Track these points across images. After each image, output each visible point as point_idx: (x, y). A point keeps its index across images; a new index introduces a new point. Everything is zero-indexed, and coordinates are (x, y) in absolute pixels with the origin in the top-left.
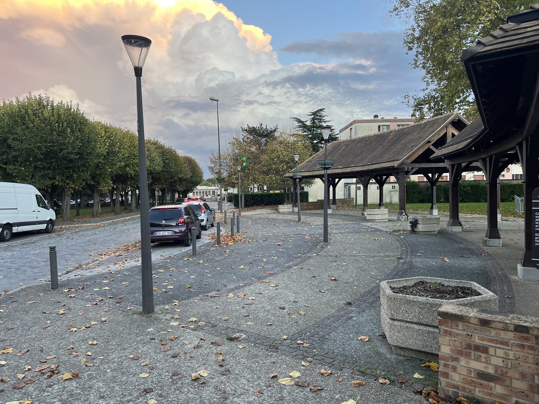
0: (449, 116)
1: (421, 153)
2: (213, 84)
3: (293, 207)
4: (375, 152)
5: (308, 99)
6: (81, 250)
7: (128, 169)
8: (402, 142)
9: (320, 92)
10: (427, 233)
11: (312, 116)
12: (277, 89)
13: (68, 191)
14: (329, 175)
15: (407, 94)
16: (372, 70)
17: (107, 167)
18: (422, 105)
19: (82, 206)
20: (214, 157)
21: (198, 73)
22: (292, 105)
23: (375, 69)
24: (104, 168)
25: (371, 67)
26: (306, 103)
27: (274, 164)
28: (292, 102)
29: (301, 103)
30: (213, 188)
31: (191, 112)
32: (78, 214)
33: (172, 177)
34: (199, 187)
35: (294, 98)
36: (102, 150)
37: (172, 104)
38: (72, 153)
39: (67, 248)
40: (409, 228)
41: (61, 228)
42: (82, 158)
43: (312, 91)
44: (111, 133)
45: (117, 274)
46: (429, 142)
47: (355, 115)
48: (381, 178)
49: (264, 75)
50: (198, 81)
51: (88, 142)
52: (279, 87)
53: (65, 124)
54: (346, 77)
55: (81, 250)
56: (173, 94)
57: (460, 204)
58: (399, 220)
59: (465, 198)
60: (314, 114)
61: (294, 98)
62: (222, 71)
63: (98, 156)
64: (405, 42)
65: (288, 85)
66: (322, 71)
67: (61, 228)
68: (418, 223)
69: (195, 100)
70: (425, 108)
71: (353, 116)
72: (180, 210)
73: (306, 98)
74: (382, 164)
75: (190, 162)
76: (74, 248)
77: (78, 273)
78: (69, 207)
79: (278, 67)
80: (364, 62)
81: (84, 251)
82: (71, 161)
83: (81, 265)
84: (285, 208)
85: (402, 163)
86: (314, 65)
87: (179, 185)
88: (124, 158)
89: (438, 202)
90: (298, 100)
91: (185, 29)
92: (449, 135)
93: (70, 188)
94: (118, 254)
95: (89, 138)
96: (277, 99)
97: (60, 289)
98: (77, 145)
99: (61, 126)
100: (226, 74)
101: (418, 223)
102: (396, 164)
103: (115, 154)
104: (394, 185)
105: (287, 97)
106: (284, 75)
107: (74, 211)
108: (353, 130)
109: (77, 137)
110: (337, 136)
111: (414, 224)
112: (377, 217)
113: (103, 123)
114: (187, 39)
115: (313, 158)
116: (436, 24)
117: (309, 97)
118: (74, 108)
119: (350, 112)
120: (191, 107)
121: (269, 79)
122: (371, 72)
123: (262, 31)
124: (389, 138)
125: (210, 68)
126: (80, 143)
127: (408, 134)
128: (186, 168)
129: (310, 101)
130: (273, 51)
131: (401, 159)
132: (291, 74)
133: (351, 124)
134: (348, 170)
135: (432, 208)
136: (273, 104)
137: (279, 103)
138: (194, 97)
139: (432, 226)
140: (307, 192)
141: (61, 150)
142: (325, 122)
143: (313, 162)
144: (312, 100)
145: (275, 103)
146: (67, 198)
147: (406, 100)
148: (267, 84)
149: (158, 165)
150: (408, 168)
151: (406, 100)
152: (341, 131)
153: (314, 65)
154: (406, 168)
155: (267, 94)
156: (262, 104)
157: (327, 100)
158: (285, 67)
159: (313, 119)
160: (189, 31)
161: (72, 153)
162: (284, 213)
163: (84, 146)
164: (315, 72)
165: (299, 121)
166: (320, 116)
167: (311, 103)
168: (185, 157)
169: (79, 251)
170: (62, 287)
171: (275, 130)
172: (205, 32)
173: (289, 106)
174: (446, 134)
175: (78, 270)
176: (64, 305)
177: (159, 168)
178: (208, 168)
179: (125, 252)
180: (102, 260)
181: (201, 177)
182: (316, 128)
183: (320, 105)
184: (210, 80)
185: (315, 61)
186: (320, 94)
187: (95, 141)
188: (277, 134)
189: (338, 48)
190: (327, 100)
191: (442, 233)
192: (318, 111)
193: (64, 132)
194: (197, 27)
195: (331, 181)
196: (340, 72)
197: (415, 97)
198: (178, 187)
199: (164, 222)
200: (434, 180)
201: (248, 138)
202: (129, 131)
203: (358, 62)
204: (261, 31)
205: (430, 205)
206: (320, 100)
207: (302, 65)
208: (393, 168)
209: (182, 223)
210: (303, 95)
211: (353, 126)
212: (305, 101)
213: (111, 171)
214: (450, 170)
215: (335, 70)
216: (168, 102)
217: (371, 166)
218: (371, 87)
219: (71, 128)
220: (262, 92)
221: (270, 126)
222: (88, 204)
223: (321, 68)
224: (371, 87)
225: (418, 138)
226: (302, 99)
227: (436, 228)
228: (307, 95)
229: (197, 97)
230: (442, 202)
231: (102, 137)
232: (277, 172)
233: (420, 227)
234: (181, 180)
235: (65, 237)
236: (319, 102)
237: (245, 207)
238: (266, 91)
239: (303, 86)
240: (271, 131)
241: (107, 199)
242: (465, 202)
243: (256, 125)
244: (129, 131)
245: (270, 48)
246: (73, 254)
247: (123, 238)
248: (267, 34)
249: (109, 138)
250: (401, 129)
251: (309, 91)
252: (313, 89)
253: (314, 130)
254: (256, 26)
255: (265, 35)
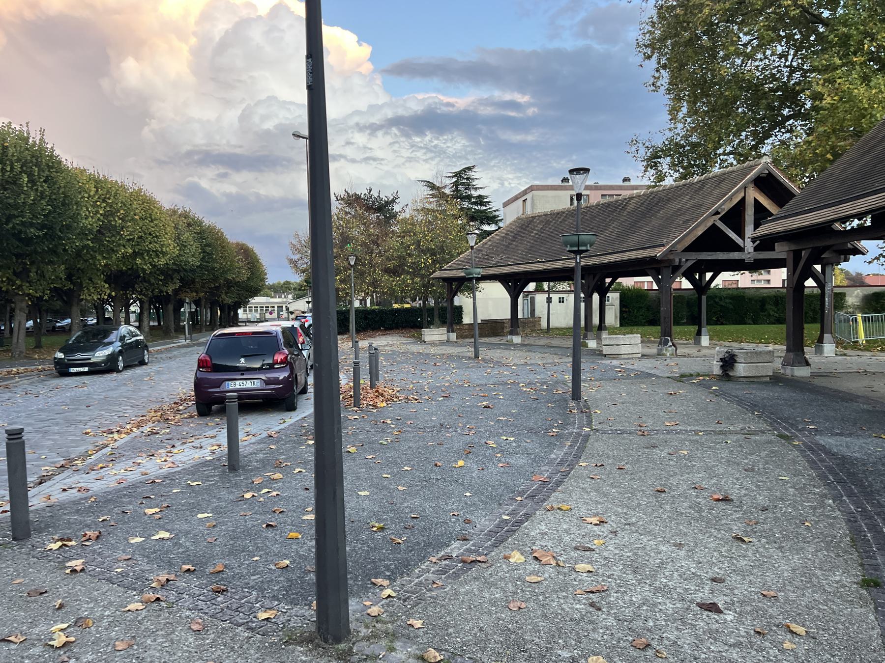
0: (751, 168)
1: (700, 233)
2: (269, 125)
3: (448, 332)
4: (607, 233)
5: (429, 155)
6: (61, 421)
7: (139, 261)
8: (659, 215)
9: (449, 145)
10: (752, 380)
11: (455, 179)
12: (376, 137)
13: (22, 301)
14: (587, 271)
15: (634, 138)
16: (531, 111)
17: (99, 257)
18: (660, 157)
19: (44, 331)
20: (300, 242)
21: (244, 106)
22: (403, 164)
23: (536, 110)
24: (94, 258)
25: (530, 105)
26: (426, 161)
27: (410, 255)
28: (404, 160)
29: (418, 161)
30: (277, 300)
31: (229, 171)
32: (38, 346)
33: (216, 279)
34: (258, 300)
35: (406, 153)
36: (90, 220)
37: (196, 157)
38: (32, 225)
39: (29, 416)
40: (717, 370)
41: (9, 373)
42: (51, 236)
43: (436, 142)
44: (108, 192)
45: (171, 486)
46: (717, 213)
47: (506, 184)
48: (702, 276)
49: (357, 113)
50: (244, 117)
51: (64, 204)
52: (380, 133)
53: (17, 166)
54: (490, 121)
55: (61, 421)
56: (200, 140)
57: (806, 326)
58: (660, 354)
59: (721, 317)
60: (458, 175)
61: (406, 153)
62: (284, 102)
63: (83, 234)
64: (638, 46)
65: (394, 130)
66: (451, 109)
67: (9, 373)
68: (735, 362)
69: (238, 151)
70: (665, 163)
71: (503, 184)
72: (276, 337)
73: (425, 153)
74: (628, 253)
75: (247, 254)
76: (44, 416)
77: (69, 482)
78: (23, 333)
79: (382, 99)
80: (522, 99)
81: (69, 423)
82: (28, 241)
83: (71, 460)
84: (434, 334)
85: (670, 251)
86: (441, 97)
87: (226, 294)
88: (132, 240)
89: (708, 324)
90: (412, 155)
91: (221, 27)
92: (750, 202)
93: (25, 295)
94: (146, 429)
95: (66, 197)
96: (379, 154)
97: (35, 539)
98: (43, 210)
99: (8, 169)
100: (292, 108)
101: (735, 362)
102: (659, 252)
103: (116, 231)
104: (561, 295)
105: (395, 151)
106: (389, 113)
107: (32, 340)
108: (529, 202)
109: (42, 193)
110: (497, 213)
111: (728, 362)
112: (624, 350)
113: (91, 171)
114: (223, 46)
115: (483, 245)
116: (701, 12)
117: (431, 151)
118: (35, 137)
119: (498, 179)
120: (232, 162)
121: (362, 120)
122: (530, 114)
123: (355, 38)
124: (630, 208)
125: (263, 97)
126: (48, 205)
127: (669, 200)
128: (239, 261)
129: (432, 159)
130: (374, 71)
131: (667, 244)
132: (401, 112)
133: (525, 192)
134: (558, 265)
135: (699, 333)
136: (371, 162)
137: (382, 159)
138: (235, 146)
139: (762, 367)
140: (461, 307)
141: (9, 218)
142: (476, 189)
143: (484, 252)
144: (435, 157)
145: (374, 159)
146: (20, 316)
147: (634, 148)
148: (361, 128)
149: (193, 256)
150: (680, 260)
151: (634, 148)
152: (505, 205)
153: (441, 97)
154: (677, 260)
155: (361, 145)
156: (353, 161)
157: (460, 157)
158: (394, 99)
159: (456, 184)
160: (227, 32)
161: (32, 225)
162: (433, 343)
163: (55, 212)
164: (439, 111)
165: (432, 186)
166: (468, 179)
167: (434, 163)
168: (238, 244)
169: (57, 424)
170: (40, 531)
171: (393, 201)
172: (256, 34)
173: (398, 166)
174: (744, 199)
175: (66, 473)
176: (61, 606)
177: (194, 261)
178: (287, 262)
179: (161, 425)
180: (116, 445)
181: (263, 280)
182: (461, 199)
183: (449, 165)
184: (265, 118)
185: (438, 90)
186: (448, 147)
187: (77, 203)
188: (397, 208)
189: (475, 73)
190: (460, 157)
191: (776, 379)
192: (464, 170)
193: (15, 183)
194: (242, 25)
195: (515, 284)
196: (480, 112)
197: (647, 144)
198: (223, 296)
199: (243, 360)
200: (704, 284)
201: (347, 213)
202: (140, 190)
203: (508, 97)
204: (354, 38)
205: (694, 329)
206: (448, 157)
207: (420, 98)
208: (653, 260)
209: (281, 362)
210: (421, 148)
211: (528, 196)
212: (424, 158)
213: (106, 265)
214: (790, 262)
215: (471, 108)
216: (189, 154)
217: (604, 257)
218: (530, 138)
219: (30, 175)
220: (352, 141)
221: (386, 195)
222: (54, 327)
223: (448, 104)
224: (530, 138)
225: (694, 206)
226: (419, 154)
227: (767, 370)
228: (428, 150)
229: (241, 147)
230: (683, 324)
231: (89, 196)
232: (416, 271)
233: (741, 369)
234: (229, 284)
235: (19, 390)
236: (447, 161)
237: (358, 331)
238: (360, 139)
239: (420, 132)
240: (386, 202)
241: (89, 319)
242: (722, 324)
243: (362, 191)
244: (140, 190)
245: (368, 67)
246: (46, 432)
247: (145, 394)
248: (364, 44)
249: (104, 201)
250: (652, 193)
251: (431, 141)
252: (438, 139)
253: (461, 199)
254: (344, 28)
255: (360, 45)
